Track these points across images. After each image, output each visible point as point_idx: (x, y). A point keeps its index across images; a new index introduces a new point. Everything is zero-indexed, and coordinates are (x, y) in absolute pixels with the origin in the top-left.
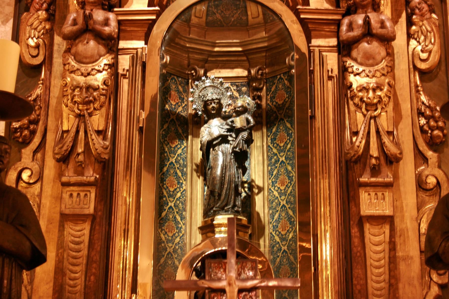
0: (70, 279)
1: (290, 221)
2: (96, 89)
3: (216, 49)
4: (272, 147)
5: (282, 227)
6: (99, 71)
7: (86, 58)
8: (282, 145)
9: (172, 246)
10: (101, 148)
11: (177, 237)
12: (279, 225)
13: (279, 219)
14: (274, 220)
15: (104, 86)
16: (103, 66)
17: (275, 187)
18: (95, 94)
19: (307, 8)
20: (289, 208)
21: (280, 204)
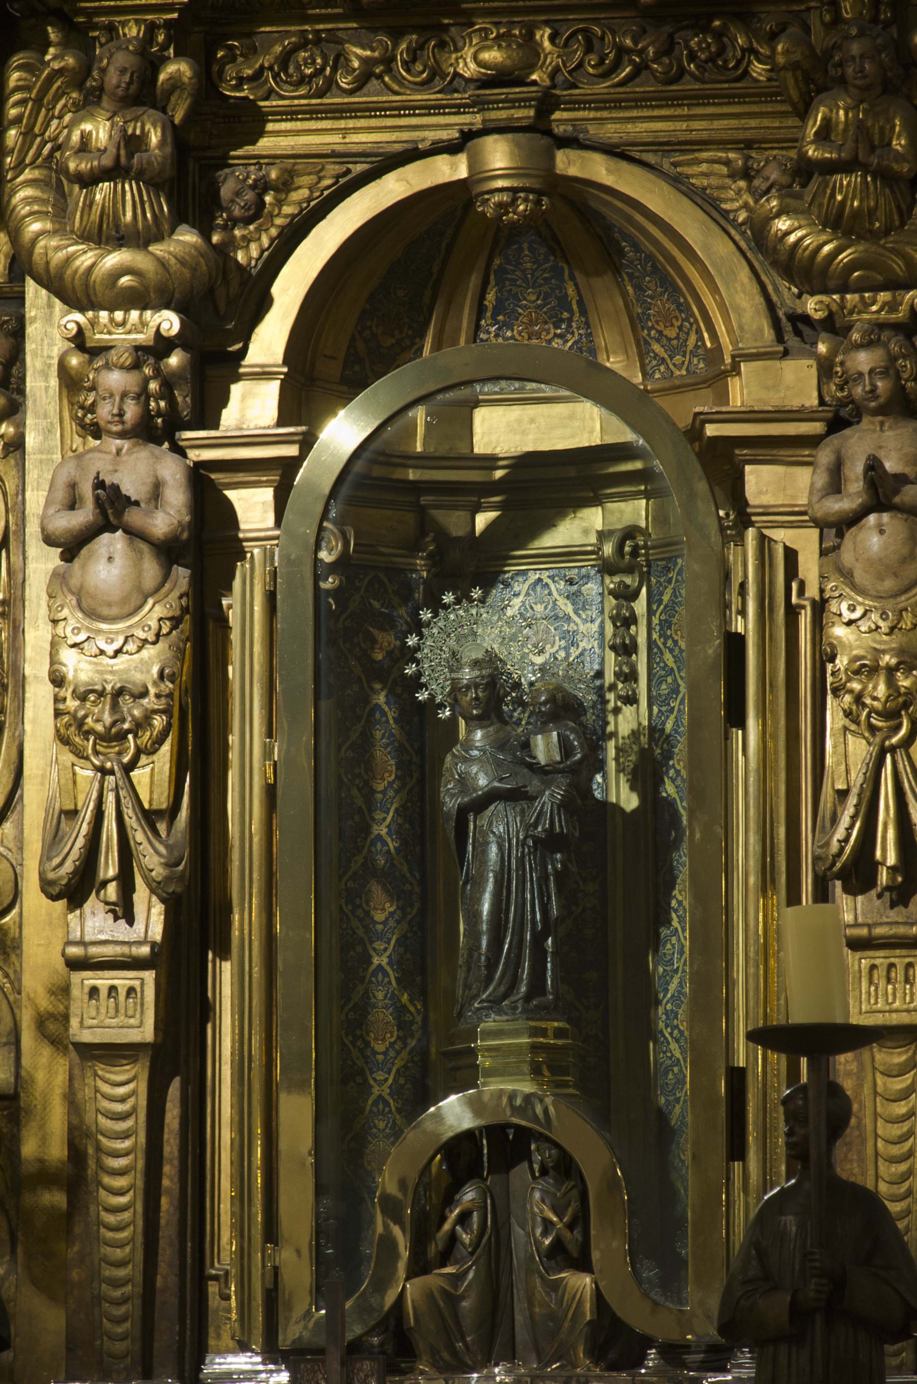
0: (107, 1210)
14: (669, 995)
17: (666, 638)
19: (724, 409)
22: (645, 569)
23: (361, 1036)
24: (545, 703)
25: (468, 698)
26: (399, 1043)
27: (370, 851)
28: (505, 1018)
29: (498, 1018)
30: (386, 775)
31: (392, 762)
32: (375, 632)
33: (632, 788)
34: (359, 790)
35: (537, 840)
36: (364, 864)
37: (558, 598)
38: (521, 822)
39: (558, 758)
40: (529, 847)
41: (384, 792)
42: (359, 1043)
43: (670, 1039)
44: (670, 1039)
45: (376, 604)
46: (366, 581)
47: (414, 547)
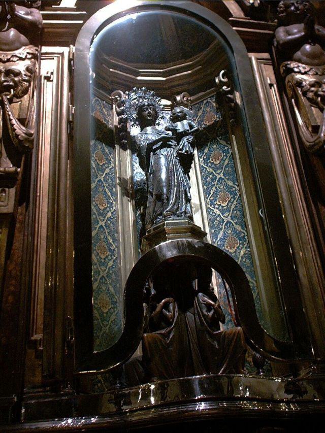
2: (18, 74)
3: (139, 78)
4: (206, 167)
5: (229, 244)
6: (21, 59)
7: (6, 44)
9: (105, 270)
10: (23, 135)
11: (110, 260)
13: (224, 236)
14: (219, 239)
15: (27, 73)
16: (25, 54)
17: (215, 205)
18: (16, 79)
21: (223, 222)
43: (213, 209)
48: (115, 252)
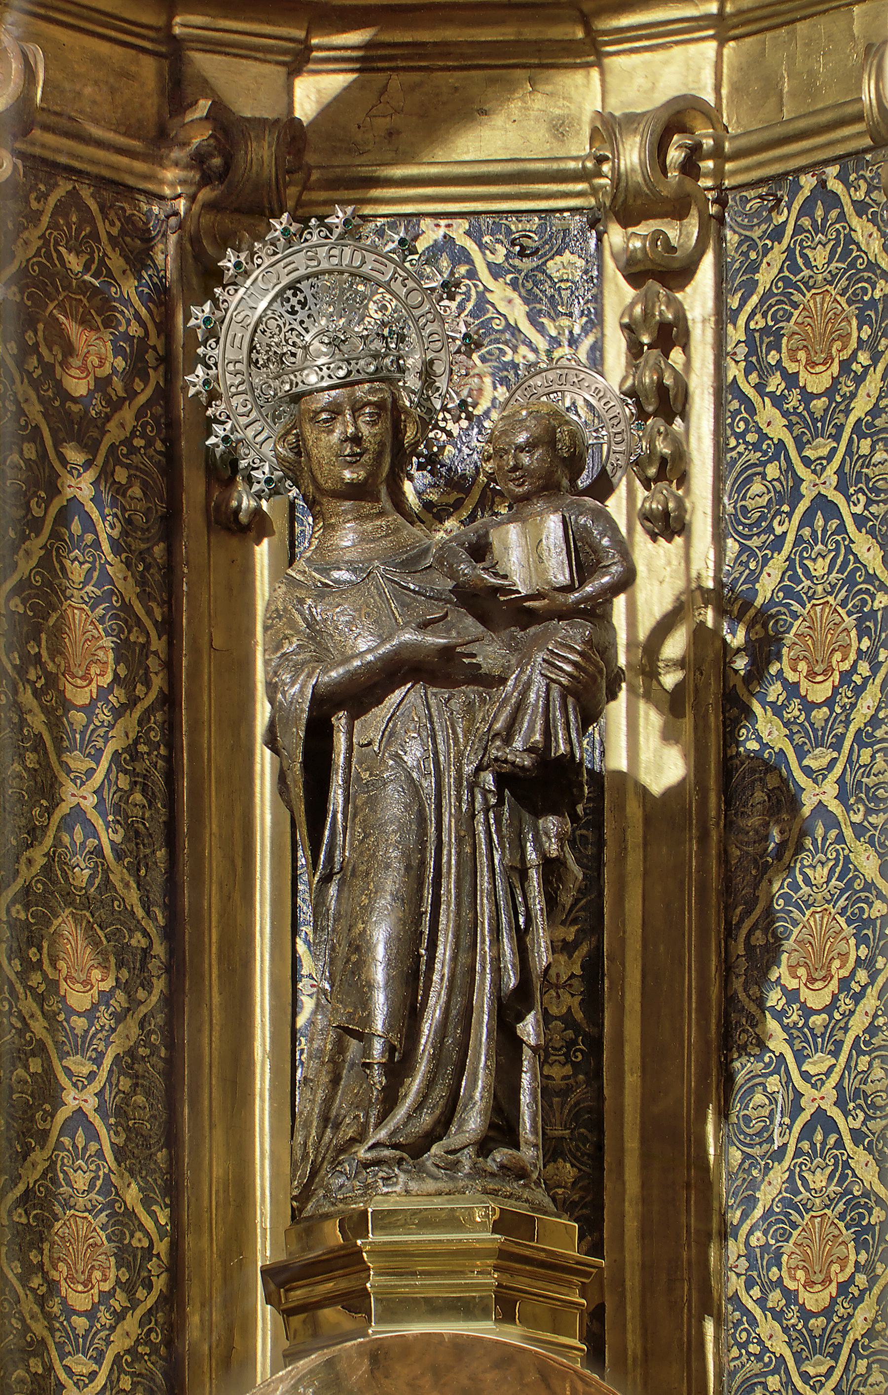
1: (855, 1222)
8: (820, 692)
12: (788, 1247)
13: (788, 1203)
14: (758, 1213)
17: (764, 372)
20: (857, 1136)
22: (713, 210)
23: (41, 1265)
24: (530, 446)
25: (336, 436)
26: (120, 1295)
27: (58, 842)
28: (431, 1185)
29: (413, 1186)
30: (95, 670)
31: (108, 642)
32: (72, 328)
33: (669, 735)
34: (36, 694)
35: (508, 779)
36: (47, 869)
37: (490, 283)
38: (467, 732)
39: (562, 578)
40: (485, 792)
41: (89, 709)
42: (36, 1281)
43: (758, 1312)
44: (758, 1312)
45: (74, 263)
46: (52, 201)
47: (160, 139)
48: (151, 1265)
